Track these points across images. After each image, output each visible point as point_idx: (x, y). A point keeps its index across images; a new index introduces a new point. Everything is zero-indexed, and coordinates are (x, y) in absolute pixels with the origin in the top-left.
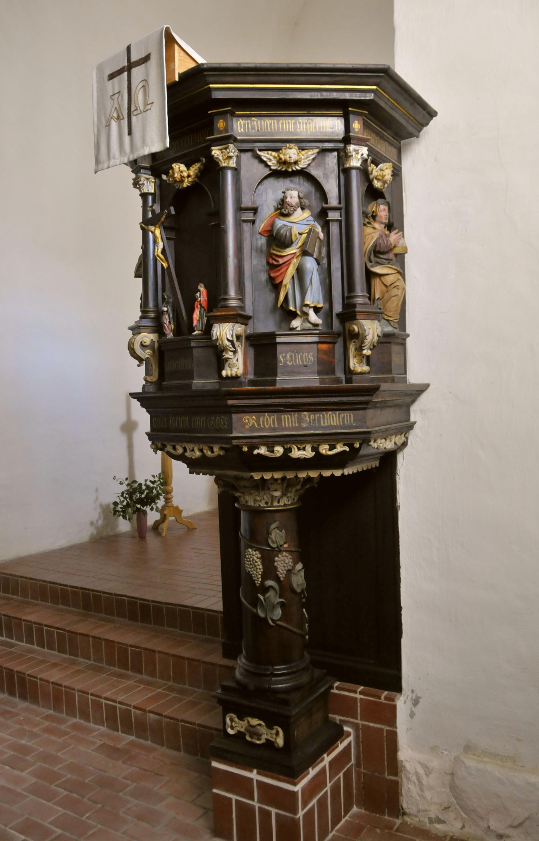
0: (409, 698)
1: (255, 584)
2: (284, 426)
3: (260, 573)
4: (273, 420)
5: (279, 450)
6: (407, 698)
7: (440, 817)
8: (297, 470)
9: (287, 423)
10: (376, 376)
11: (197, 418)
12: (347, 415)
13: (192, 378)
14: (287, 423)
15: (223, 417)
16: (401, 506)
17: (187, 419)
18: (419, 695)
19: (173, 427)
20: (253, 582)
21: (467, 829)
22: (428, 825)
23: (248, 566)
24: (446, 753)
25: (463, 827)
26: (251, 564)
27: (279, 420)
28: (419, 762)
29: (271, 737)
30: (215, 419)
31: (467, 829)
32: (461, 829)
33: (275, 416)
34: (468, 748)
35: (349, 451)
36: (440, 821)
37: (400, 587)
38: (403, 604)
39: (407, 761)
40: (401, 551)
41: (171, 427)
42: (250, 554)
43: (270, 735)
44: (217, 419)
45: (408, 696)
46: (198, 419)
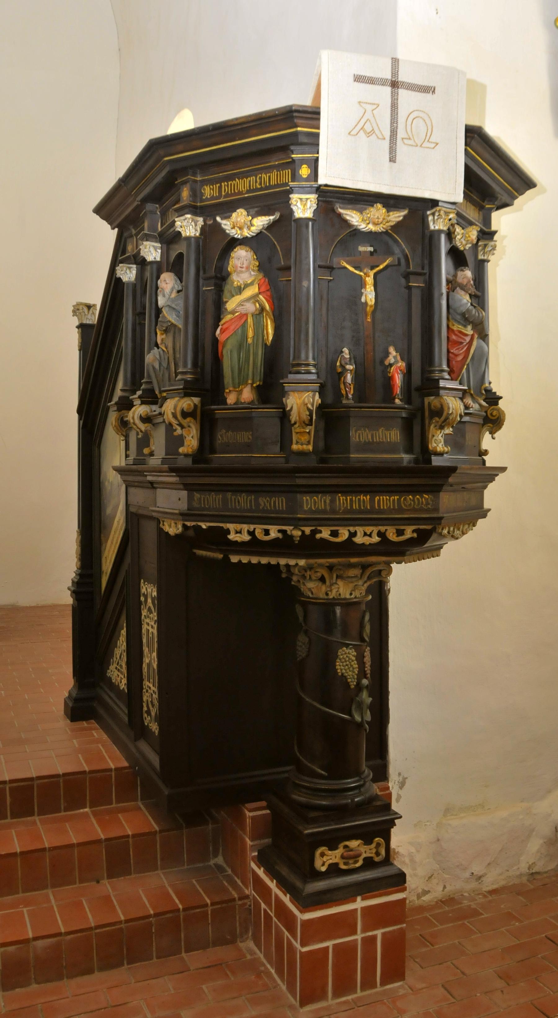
0: (396, 782)
1: (349, 686)
2: (230, 507)
3: (357, 672)
4: (251, 501)
5: (344, 534)
6: (395, 783)
7: (425, 889)
8: (289, 558)
9: (233, 505)
10: (248, 455)
11: (385, 497)
12: (383, 498)
13: (349, 453)
14: (233, 505)
15: (427, 496)
16: (391, 589)
17: (367, 498)
18: (405, 777)
19: (342, 509)
20: (347, 685)
21: (448, 888)
22: (417, 902)
23: (340, 667)
24: (428, 824)
25: (445, 887)
26: (347, 665)
27: (333, 501)
28: (411, 843)
29: (370, 853)
30: (271, 500)
31: (448, 888)
32: (443, 891)
33: (328, 498)
34: (448, 811)
35: (282, 538)
36: (425, 892)
37: (388, 672)
38: (390, 689)
39: (398, 846)
40: (390, 635)
41: (338, 509)
42: (346, 653)
43: (370, 851)
44: (314, 499)
45: (395, 781)
46: (387, 499)
